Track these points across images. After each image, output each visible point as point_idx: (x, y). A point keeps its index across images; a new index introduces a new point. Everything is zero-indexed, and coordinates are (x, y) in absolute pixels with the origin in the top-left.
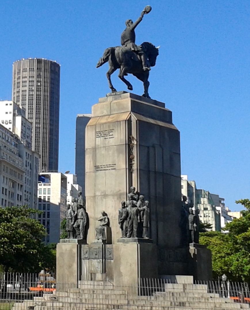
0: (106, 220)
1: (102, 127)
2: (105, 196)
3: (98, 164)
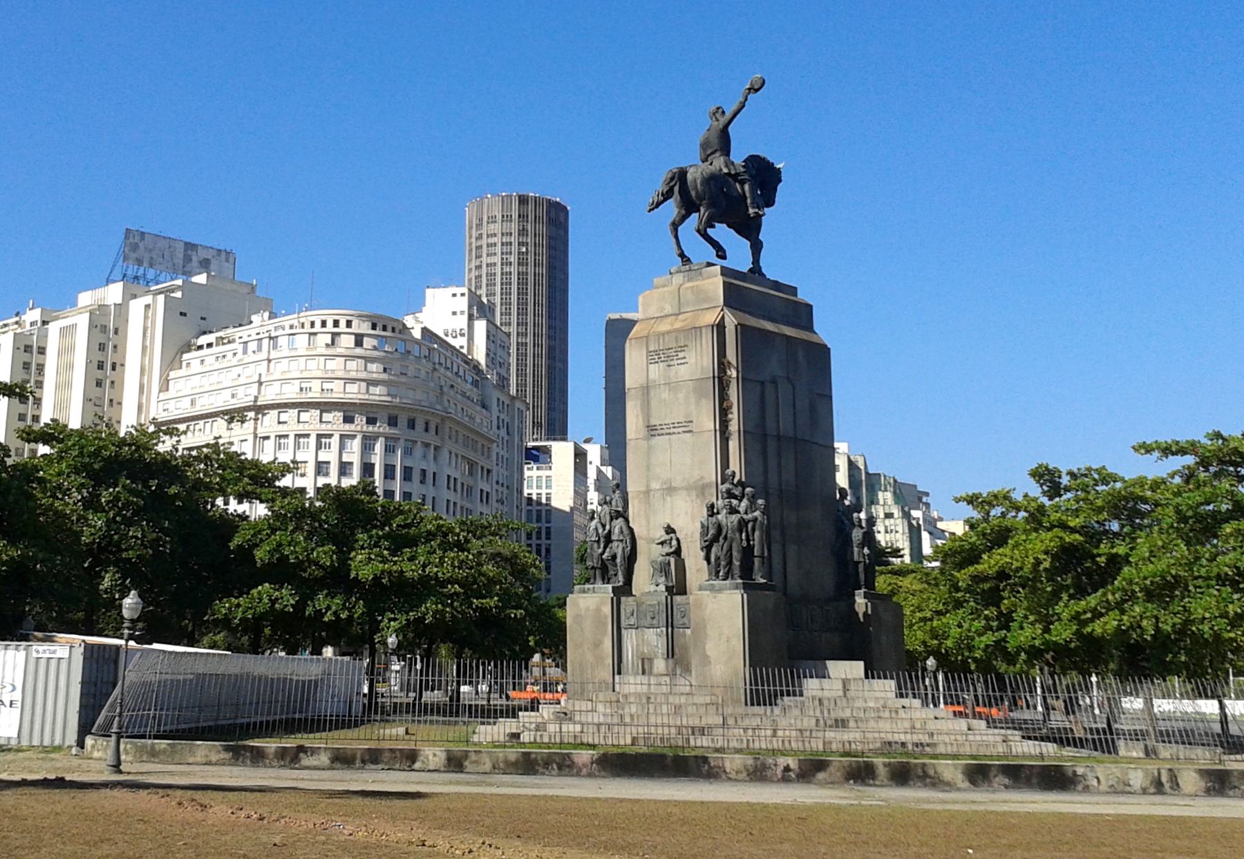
0: (674, 543)
1: (661, 341)
2: (670, 490)
3: (653, 422)
